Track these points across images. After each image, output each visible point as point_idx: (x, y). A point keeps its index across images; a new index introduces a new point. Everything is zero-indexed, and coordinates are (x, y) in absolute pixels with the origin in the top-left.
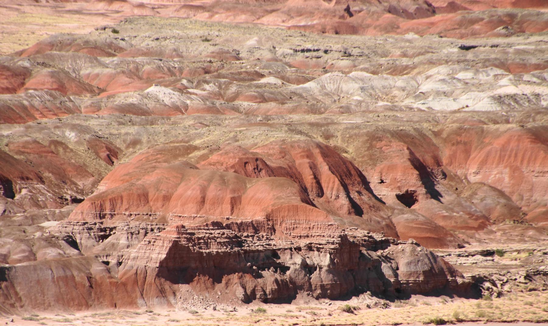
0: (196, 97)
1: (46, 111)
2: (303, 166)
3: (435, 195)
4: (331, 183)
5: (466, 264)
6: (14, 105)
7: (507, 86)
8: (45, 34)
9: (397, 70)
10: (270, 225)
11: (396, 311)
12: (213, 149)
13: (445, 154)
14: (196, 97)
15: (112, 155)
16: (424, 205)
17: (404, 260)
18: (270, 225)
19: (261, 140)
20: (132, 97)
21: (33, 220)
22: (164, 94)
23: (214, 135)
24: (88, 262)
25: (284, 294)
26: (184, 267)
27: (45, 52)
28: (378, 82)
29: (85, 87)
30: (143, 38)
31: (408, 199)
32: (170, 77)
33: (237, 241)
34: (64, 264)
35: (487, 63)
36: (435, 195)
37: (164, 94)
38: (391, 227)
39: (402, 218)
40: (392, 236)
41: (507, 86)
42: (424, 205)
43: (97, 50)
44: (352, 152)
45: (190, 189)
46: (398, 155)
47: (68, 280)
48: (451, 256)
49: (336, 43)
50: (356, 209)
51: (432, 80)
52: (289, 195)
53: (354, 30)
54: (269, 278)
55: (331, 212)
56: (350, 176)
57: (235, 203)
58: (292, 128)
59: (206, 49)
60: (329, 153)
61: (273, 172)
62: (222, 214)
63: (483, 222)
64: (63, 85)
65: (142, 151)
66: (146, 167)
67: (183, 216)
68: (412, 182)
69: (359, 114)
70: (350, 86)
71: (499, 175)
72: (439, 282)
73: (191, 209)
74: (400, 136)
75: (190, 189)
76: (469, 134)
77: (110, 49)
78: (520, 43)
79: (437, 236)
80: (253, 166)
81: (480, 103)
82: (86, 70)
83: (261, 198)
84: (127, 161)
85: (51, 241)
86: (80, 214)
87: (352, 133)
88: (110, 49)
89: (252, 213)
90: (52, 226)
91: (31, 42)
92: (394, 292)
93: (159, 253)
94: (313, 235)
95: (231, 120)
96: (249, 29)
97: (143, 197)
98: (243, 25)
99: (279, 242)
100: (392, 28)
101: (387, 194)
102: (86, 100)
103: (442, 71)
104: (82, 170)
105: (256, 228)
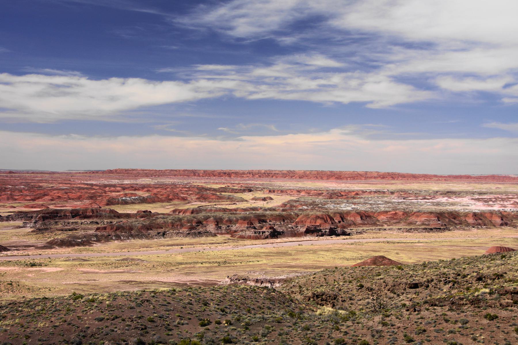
0: (310, 207)
1: (289, 210)
2: (325, 217)
3: (343, 221)
4: (329, 220)
5: (348, 231)
6: (93, 244)
7: (353, 206)
8: (289, 199)
9: (338, 204)
10: (320, 226)
11: (338, 238)
12: (312, 215)
13: (345, 216)
14: (310, 207)
15: (298, 216)
16: (342, 223)
17: (339, 230)
18: (320, 226)
19: (319, 214)
20: (301, 208)
21: (287, 225)
22: (305, 207)
23: (312, 213)
24: (294, 231)
25: (322, 235)
26: (309, 232)
27: (289, 202)
28: (335, 206)
29: (294, 206)
30: (302, 200)
31: (340, 222)
32: (306, 205)
33: (315, 228)
34: (291, 231)
35: (350, 203)
36: (343, 221)
37: (305, 207)
38: (337, 226)
39: (339, 225)
40: (338, 227)
41: (353, 206)
42: (342, 223)
43: (296, 201)
44: (332, 215)
45: (309, 221)
46: (338, 216)
47: (292, 233)
48: (346, 230)
49: (329, 200)
50: (332, 223)
51: (343, 205)
52: (323, 221)
53: (332, 198)
54: (320, 233)
55: (329, 224)
56: (331, 219)
57: (315, 223)
58: (323, 212)
59: (311, 201)
60: (329, 216)
61: (321, 218)
62: (314, 224)
63: (350, 225)
64: (292, 206)
65: (302, 215)
66: (303, 217)
67: (308, 224)
68: (340, 220)
69: (246, 172)
70: (332, 206)
71: (352, 219)
72: (344, 234)
73: (309, 223)
74: (339, 213)
75: (309, 221)
76: (348, 213)
77: (298, 201)
78: (355, 200)
79: (344, 227)
80: (318, 217)
81: (349, 209)
82: (295, 204)
83: (319, 222)
84: (300, 217)
85: (290, 228)
86: (293, 224)
87: (332, 213)
88: (298, 201)
89: (318, 224)
90: (290, 226)
91: (287, 201)
92: (338, 235)
93: (305, 230)
94: (326, 227)
95: (315, 211)
96: (317, 198)
97: (302, 222)
98: (288, 40)
99: (321, 228)
100: (337, 198)
101: (337, 221)
102: (294, 208)
103: (344, 204)
104: (294, 218)
105: (318, 226)
